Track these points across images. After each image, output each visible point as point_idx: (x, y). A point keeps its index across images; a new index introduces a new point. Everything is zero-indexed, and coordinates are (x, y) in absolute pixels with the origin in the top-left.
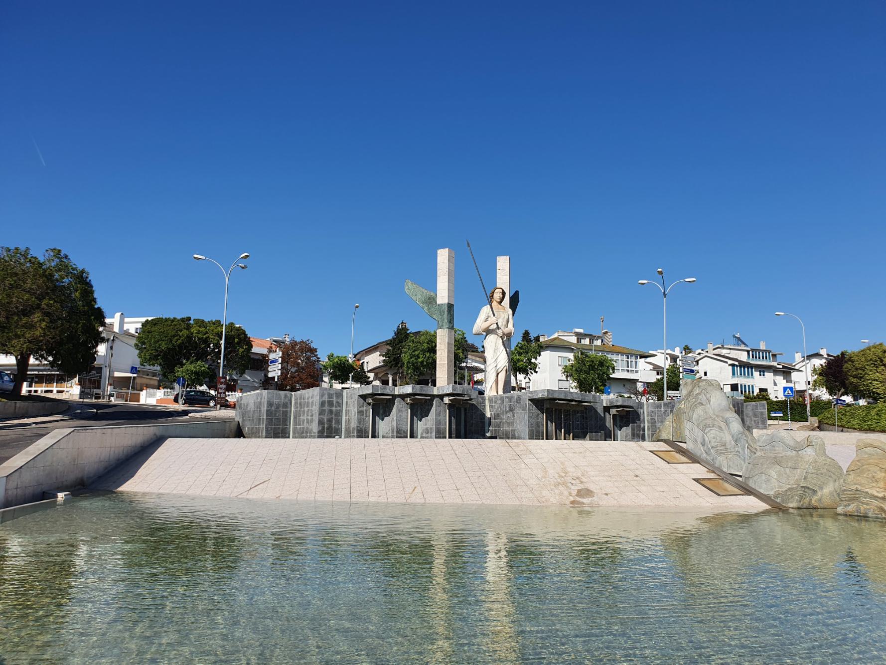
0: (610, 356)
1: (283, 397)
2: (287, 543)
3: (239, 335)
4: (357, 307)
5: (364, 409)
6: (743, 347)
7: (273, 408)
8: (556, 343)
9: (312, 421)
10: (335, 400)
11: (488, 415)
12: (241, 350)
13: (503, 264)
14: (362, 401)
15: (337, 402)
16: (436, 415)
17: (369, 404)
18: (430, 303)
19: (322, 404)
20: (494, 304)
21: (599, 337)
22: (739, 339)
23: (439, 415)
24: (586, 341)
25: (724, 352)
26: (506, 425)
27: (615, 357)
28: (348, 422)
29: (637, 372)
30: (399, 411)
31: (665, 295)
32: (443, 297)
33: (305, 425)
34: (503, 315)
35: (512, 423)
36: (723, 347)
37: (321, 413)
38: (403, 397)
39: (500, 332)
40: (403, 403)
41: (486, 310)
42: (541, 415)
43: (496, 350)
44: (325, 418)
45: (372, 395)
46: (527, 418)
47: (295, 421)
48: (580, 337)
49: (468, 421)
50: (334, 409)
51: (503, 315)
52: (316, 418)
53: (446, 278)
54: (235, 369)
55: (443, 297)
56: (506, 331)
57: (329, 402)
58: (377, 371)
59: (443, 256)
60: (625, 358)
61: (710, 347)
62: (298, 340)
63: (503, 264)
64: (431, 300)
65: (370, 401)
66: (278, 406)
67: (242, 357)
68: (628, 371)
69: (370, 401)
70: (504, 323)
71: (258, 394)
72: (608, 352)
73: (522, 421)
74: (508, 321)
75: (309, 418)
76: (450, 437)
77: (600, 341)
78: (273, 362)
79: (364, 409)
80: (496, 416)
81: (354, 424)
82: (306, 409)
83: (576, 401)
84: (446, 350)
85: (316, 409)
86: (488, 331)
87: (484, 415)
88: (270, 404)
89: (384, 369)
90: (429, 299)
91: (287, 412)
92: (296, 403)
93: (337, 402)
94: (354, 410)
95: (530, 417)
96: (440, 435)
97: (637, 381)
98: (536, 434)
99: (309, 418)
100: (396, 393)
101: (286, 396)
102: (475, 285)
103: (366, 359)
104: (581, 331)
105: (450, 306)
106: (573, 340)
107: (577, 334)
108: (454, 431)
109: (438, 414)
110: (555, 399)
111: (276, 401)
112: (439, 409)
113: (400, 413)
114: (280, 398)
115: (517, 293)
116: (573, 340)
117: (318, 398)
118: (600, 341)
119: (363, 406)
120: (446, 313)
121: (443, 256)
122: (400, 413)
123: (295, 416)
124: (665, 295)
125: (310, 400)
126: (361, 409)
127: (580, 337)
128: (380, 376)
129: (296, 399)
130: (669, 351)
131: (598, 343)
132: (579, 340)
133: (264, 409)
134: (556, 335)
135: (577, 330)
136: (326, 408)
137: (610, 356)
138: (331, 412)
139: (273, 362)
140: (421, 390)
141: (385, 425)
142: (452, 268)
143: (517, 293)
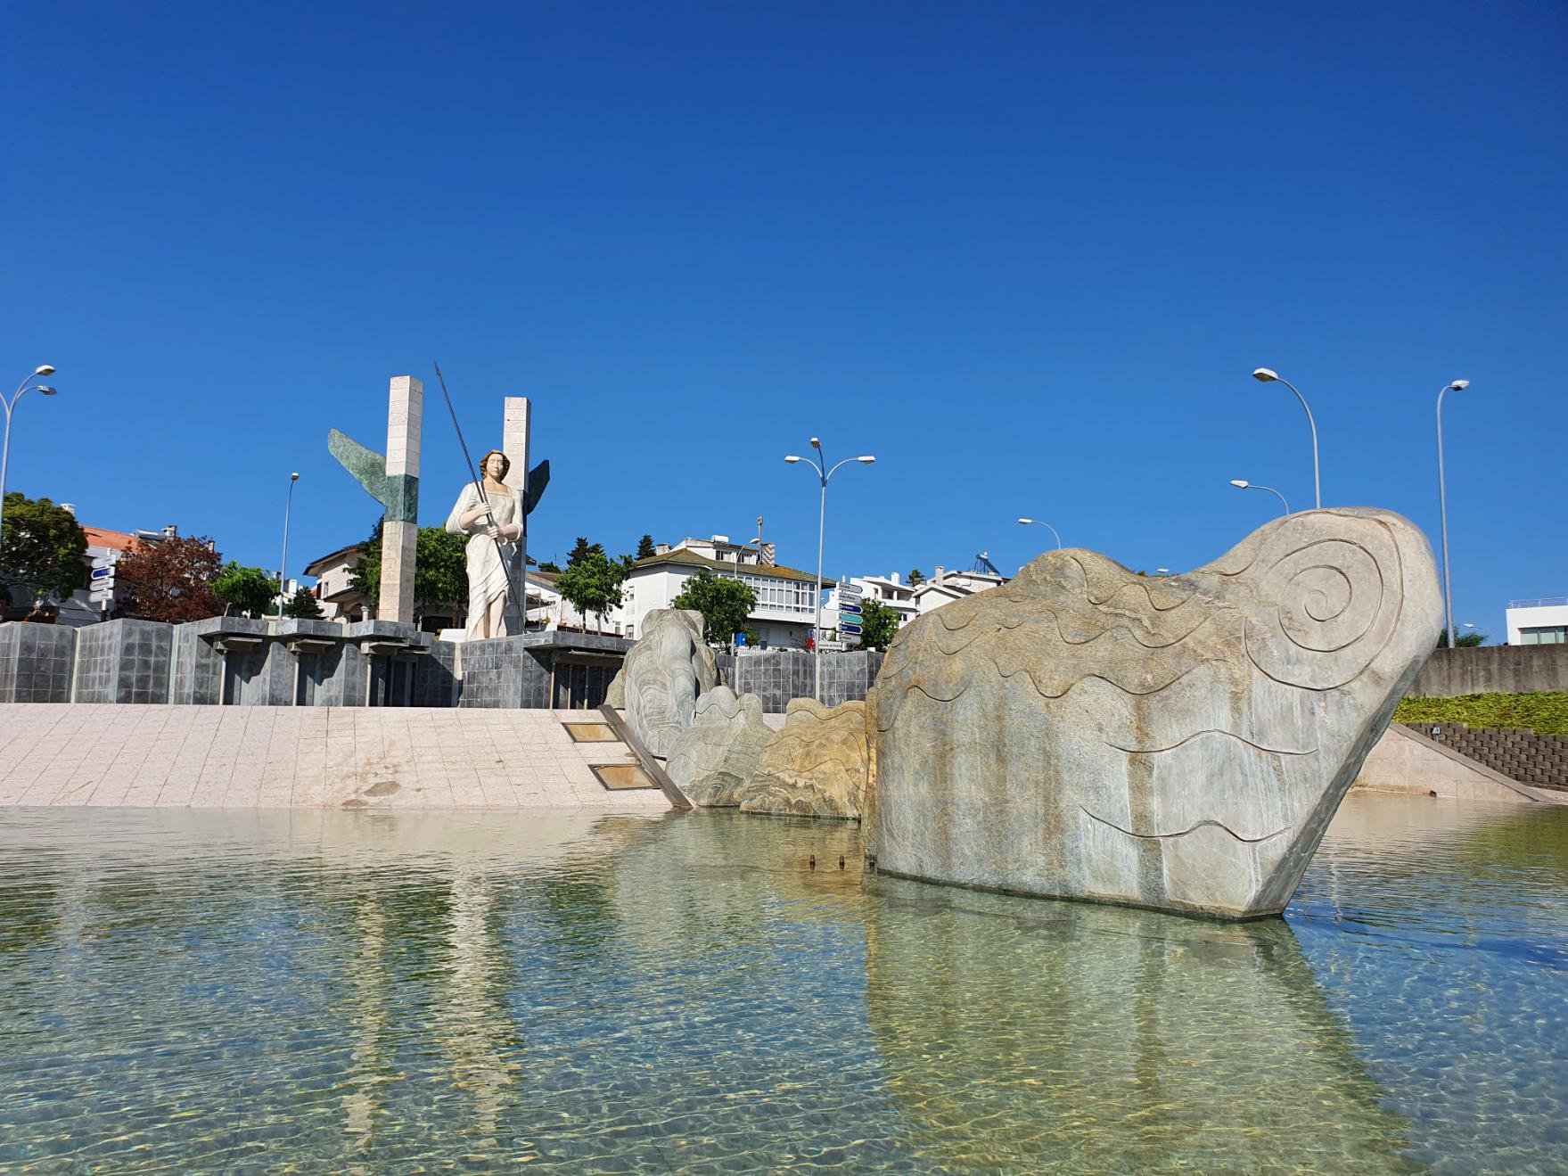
0: (752, 583)
1: (56, 635)
2: (131, 903)
3: (58, 523)
4: (295, 478)
5: (210, 661)
6: (992, 576)
7: (34, 656)
8: (680, 558)
9: (108, 680)
10: (154, 643)
11: (458, 675)
12: (62, 551)
13: (515, 411)
14: (206, 646)
15: (159, 647)
16: (347, 675)
17: (220, 652)
18: (373, 473)
19: (128, 649)
20: (489, 480)
21: (754, 552)
22: (986, 561)
23: (353, 669)
24: (732, 558)
25: (961, 582)
26: (486, 693)
27: (760, 584)
28: (180, 684)
29: (811, 611)
30: (277, 665)
31: (824, 483)
32: (396, 463)
33: (97, 689)
34: (501, 501)
35: (496, 689)
36: (959, 575)
37: (125, 666)
38: (284, 640)
39: (493, 530)
40: (285, 651)
41: (470, 491)
42: (546, 676)
43: (486, 562)
44: (134, 675)
45: (222, 636)
46: (519, 679)
47: (80, 679)
48: (721, 549)
49: (411, 677)
50: (152, 659)
51: (501, 501)
52: (115, 675)
53: (403, 429)
54: (50, 587)
55: (396, 463)
56: (506, 529)
57: (141, 646)
58: (341, 598)
59: (400, 390)
60: (793, 587)
61: (940, 573)
62: (184, 535)
63: (515, 411)
64: (376, 469)
65: (220, 646)
66: (44, 654)
67: (66, 565)
68: (798, 609)
69: (220, 646)
70: (504, 516)
71: (5, 629)
72: (749, 575)
73: (512, 681)
74: (512, 511)
75: (104, 674)
76: (373, 703)
77: (754, 558)
78: (99, 573)
79: (210, 661)
80: (472, 677)
81: (189, 688)
82: (99, 658)
83: (607, 652)
84: (399, 561)
85: (115, 658)
86: (474, 529)
87: (449, 676)
88: (27, 648)
89: (358, 594)
90: (372, 465)
91: (64, 664)
92: (83, 648)
93: (159, 647)
94: (190, 661)
95: (524, 679)
96: (350, 702)
97: (811, 626)
98: (533, 700)
99: (104, 674)
100: (271, 633)
101: (62, 634)
102: (458, 445)
103: (327, 576)
104: (725, 539)
105: (410, 482)
106: (710, 554)
107: (717, 545)
108: (381, 695)
109: (350, 672)
110: (569, 649)
111: (40, 643)
112: (352, 663)
113: (280, 667)
114: (49, 635)
115: (545, 464)
116: (710, 554)
117: (119, 638)
118: (754, 558)
119: (208, 656)
120: (401, 493)
121: (400, 390)
122: (280, 667)
123: (81, 671)
124: (824, 483)
125: (107, 642)
126: (204, 661)
127: (721, 549)
128: (348, 608)
129: (83, 641)
130: (882, 580)
131: (751, 560)
132: (719, 555)
133: (15, 656)
134: (682, 546)
135: (719, 538)
136: (136, 657)
137: (752, 583)
138: (146, 664)
139: (99, 573)
140: (315, 629)
141: (249, 689)
142: (418, 412)
143: (545, 464)
